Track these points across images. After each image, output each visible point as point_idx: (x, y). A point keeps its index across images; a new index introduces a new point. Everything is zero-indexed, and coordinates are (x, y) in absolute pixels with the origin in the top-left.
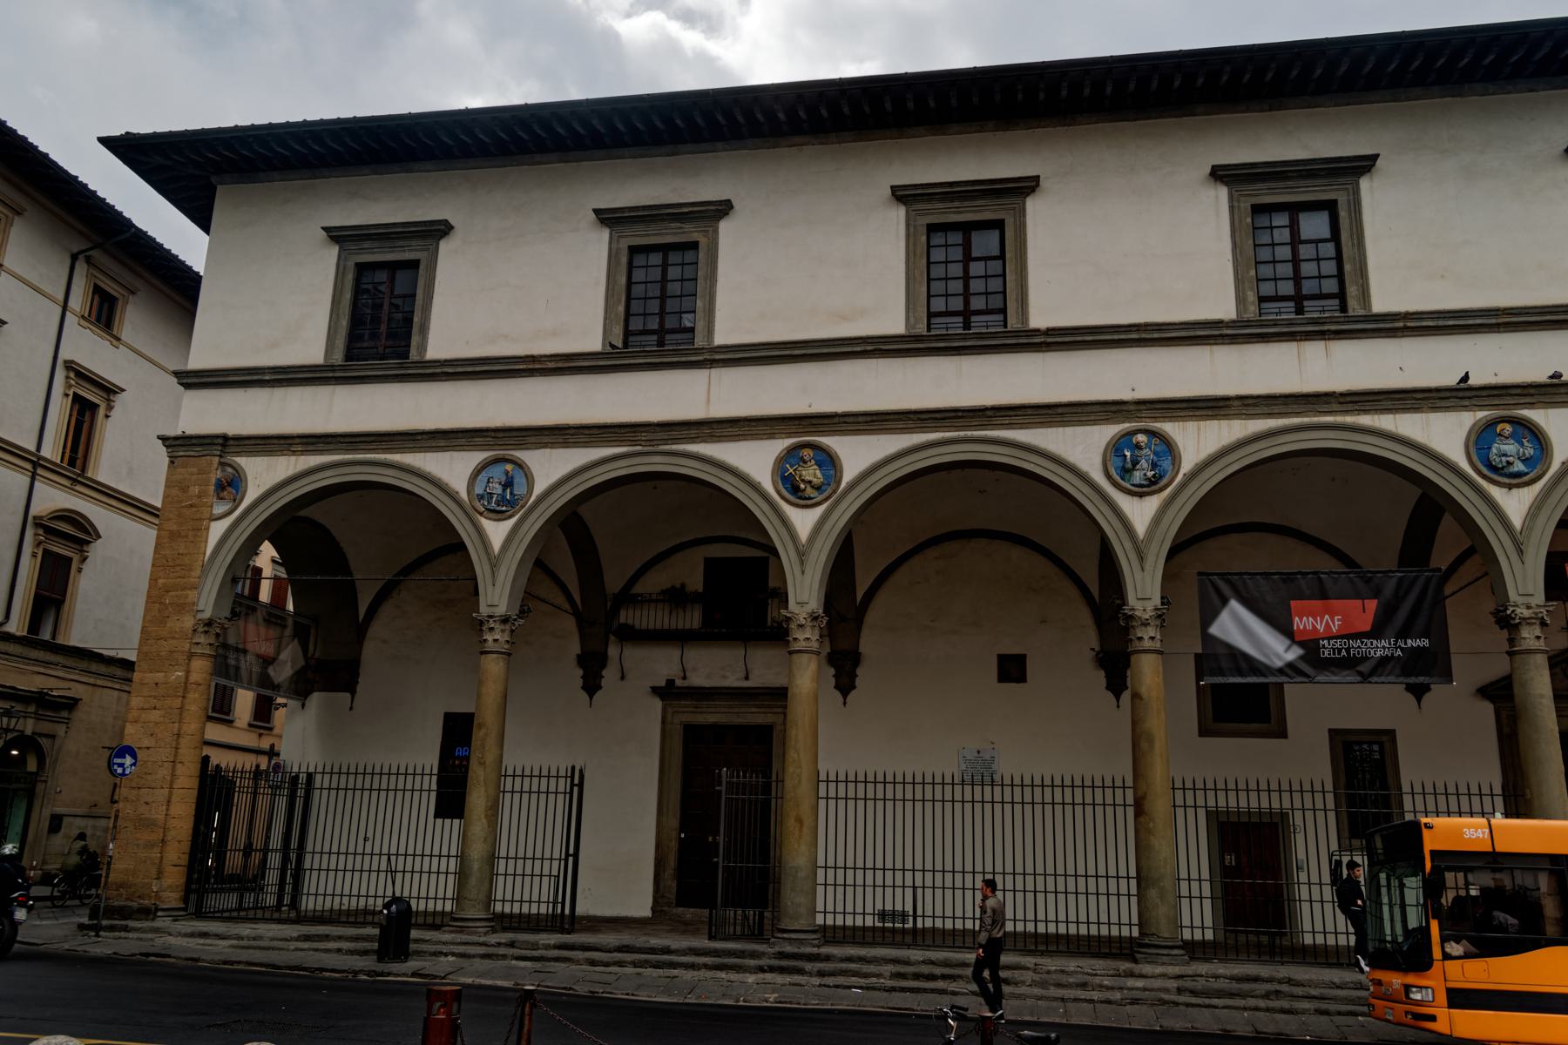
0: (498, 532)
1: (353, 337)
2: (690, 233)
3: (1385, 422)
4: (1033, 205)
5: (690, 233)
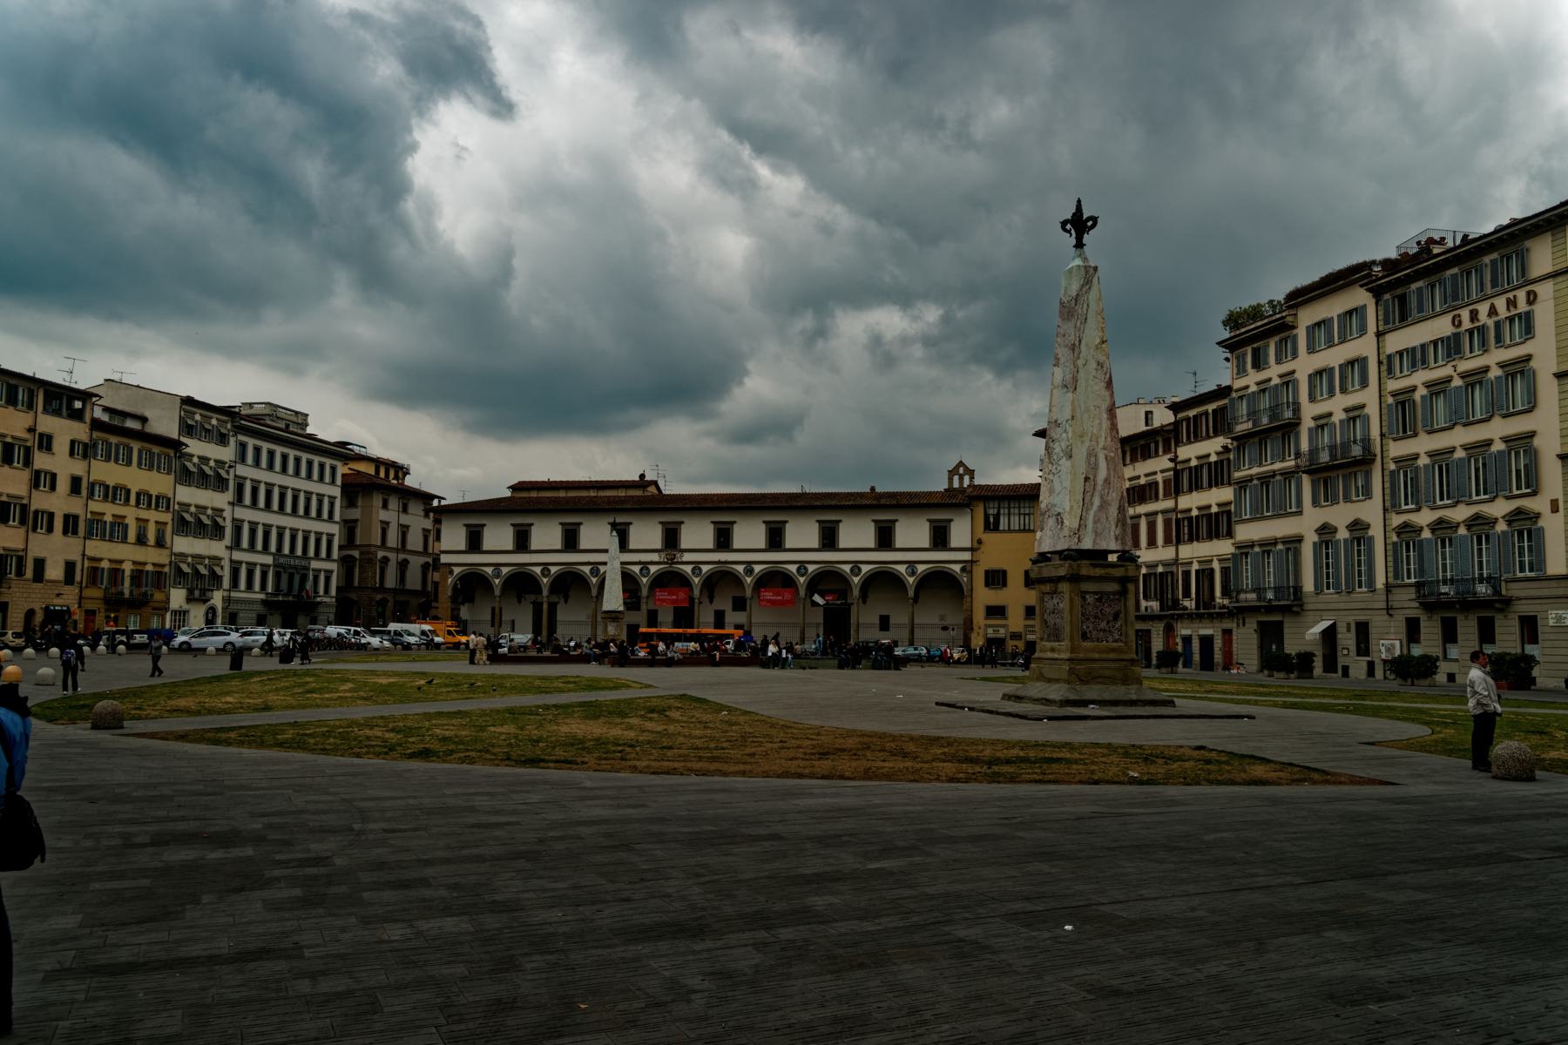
0: (497, 581)
1: (517, 545)
2: (527, 528)
3: (947, 566)
4: (631, 526)
5: (527, 528)
